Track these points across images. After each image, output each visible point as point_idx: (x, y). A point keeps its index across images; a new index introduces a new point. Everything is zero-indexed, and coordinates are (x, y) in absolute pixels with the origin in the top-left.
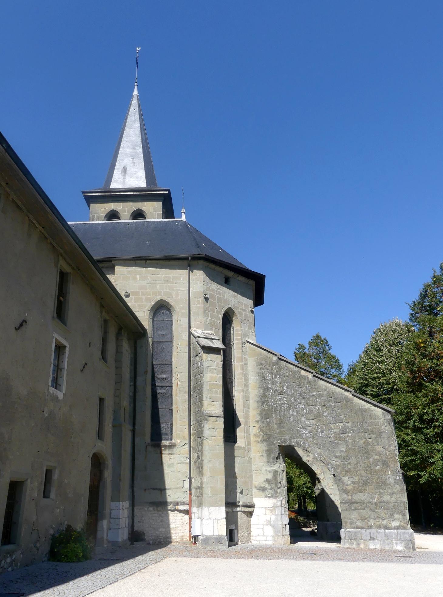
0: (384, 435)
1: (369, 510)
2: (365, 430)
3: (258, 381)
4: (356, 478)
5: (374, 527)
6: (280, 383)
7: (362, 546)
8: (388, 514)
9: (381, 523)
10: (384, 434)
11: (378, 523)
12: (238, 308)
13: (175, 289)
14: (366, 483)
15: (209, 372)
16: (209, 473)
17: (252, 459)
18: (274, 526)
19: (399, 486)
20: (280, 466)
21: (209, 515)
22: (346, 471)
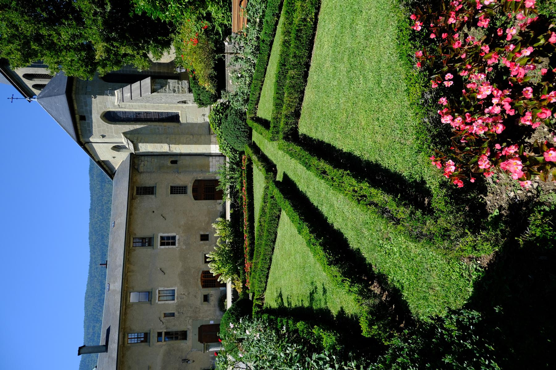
12: (98, 110)
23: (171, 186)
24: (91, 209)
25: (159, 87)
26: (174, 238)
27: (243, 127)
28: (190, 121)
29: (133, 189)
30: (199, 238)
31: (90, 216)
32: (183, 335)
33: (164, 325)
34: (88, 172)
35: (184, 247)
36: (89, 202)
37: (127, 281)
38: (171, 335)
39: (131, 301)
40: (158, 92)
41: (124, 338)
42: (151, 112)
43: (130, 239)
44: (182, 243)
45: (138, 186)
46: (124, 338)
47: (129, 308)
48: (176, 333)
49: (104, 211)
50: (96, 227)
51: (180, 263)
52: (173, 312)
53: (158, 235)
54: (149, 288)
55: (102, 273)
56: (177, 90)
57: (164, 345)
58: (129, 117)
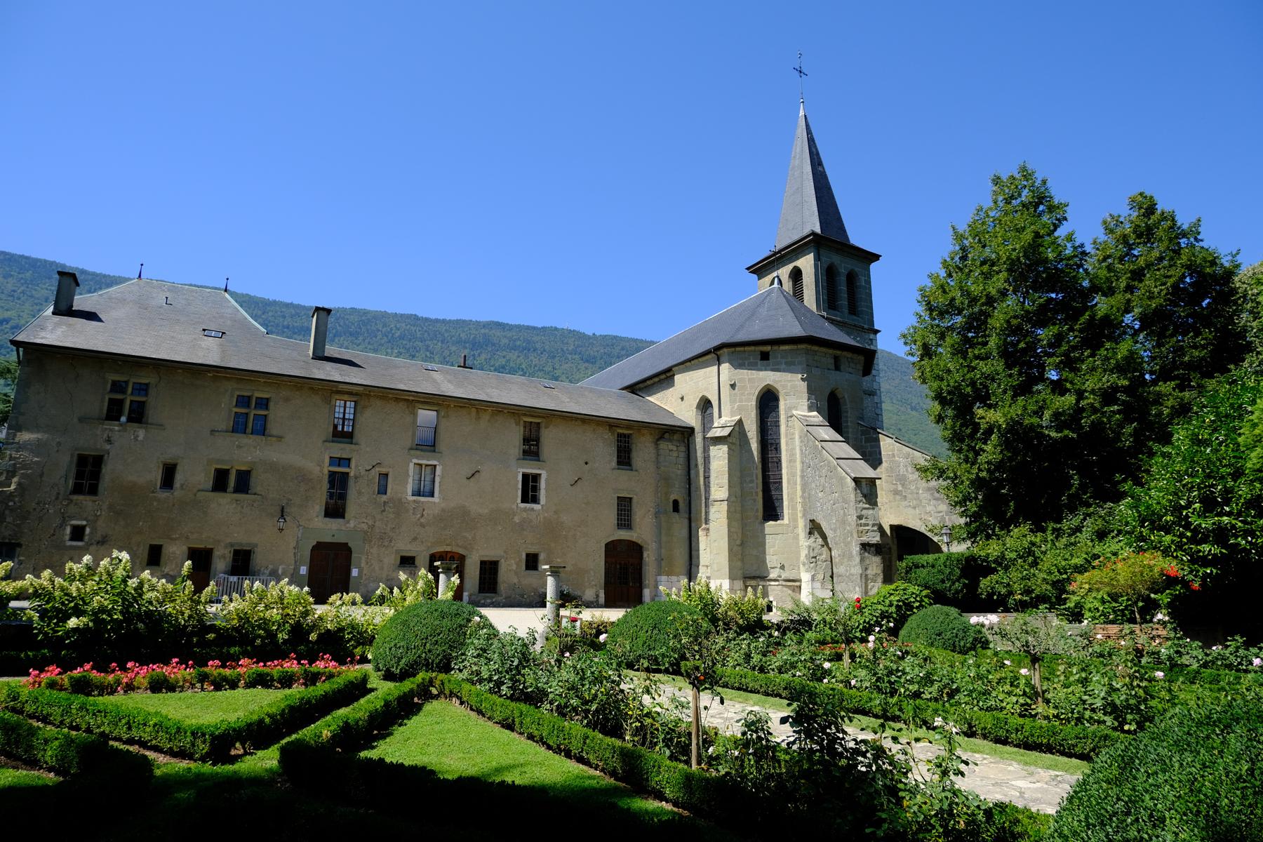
12: (781, 381)
23: (631, 499)
24: (416, 317)
25: (865, 491)
26: (535, 500)
27: (962, 644)
28: (769, 540)
29: (628, 427)
30: (532, 550)
31: (402, 315)
32: (335, 510)
33: (363, 472)
34: (496, 320)
35: (517, 519)
36: (433, 317)
37: (461, 407)
38: (338, 484)
39: (420, 411)
40: (856, 490)
41: (350, 393)
42: (781, 470)
43: (539, 417)
44: (525, 515)
45: (634, 436)
46: (350, 393)
47: (408, 407)
48: (343, 497)
49: (410, 340)
50: (376, 324)
51: (486, 511)
52: (389, 491)
53: (543, 469)
54: (441, 446)
55: (272, 326)
56: (863, 521)
57: (321, 471)
58: (770, 432)
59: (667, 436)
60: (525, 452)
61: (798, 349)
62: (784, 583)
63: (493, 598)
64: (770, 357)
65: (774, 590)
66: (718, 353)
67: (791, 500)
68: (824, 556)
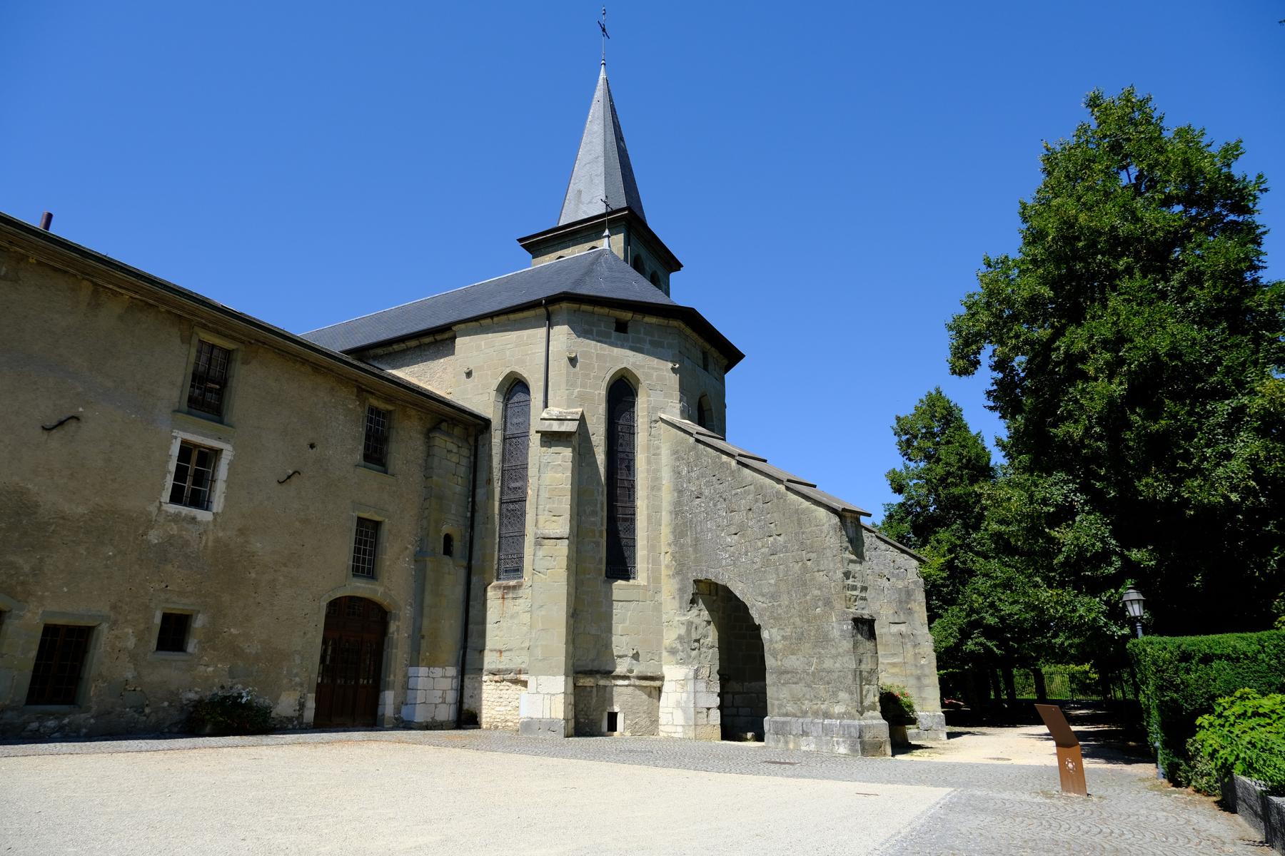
0: (828, 553)
1: (804, 685)
2: (803, 546)
3: (672, 480)
4: (788, 630)
5: (810, 714)
6: (698, 479)
7: (791, 746)
8: (829, 691)
9: (820, 707)
10: (828, 550)
11: (815, 707)
12: (643, 367)
13: (529, 352)
14: (800, 639)
15: (550, 470)
16: (540, 625)
17: (661, 603)
18: (685, 711)
19: (847, 642)
20: (700, 615)
21: (537, 688)
22: (774, 619)
25: (851, 535)
26: (199, 500)
28: (618, 609)
30: (179, 605)
35: (154, 537)
37: (55, 269)
40: (841, 529)
43: (234, 339)
44: (174, 529)
51: (81, 510)
53: (227, 442)
56: (850, 582)
58: (620, 441)
59: (444, 426)
60: (192, 401)
61: (668, 326)
62: (638, 682)
63: (65, 715)
64: (629, 329)
65: (620, 694)
66: (550, 309)
67: (653, 547)
68: (710, 639)
